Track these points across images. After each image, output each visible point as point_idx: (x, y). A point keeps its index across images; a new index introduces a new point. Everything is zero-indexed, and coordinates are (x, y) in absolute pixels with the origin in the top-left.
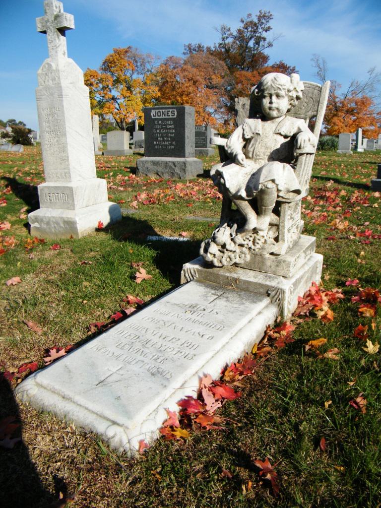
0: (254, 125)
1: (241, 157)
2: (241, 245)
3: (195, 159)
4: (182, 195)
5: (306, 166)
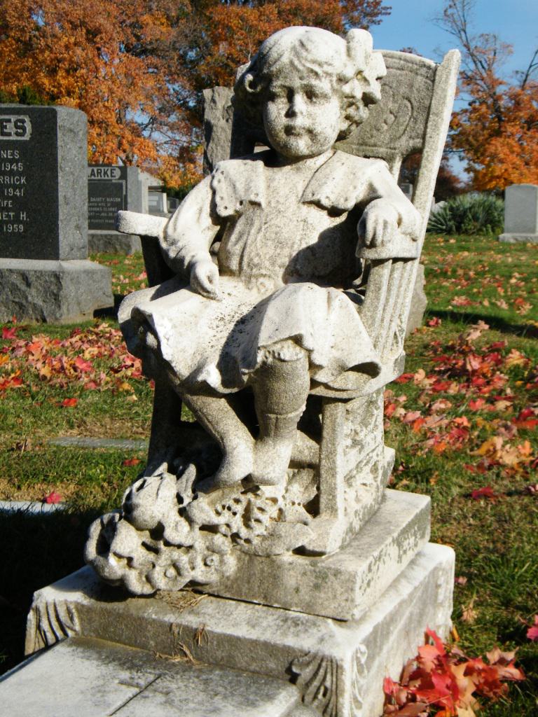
0: (241, 176)
1: (206, 268)
2: (210, 529)
3: (89, 264)
4: (45, 371)
5: (394, 292)
